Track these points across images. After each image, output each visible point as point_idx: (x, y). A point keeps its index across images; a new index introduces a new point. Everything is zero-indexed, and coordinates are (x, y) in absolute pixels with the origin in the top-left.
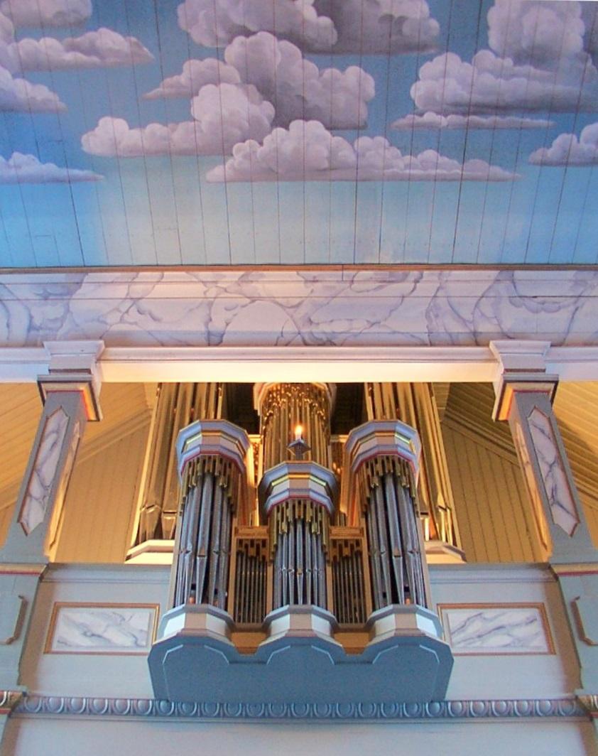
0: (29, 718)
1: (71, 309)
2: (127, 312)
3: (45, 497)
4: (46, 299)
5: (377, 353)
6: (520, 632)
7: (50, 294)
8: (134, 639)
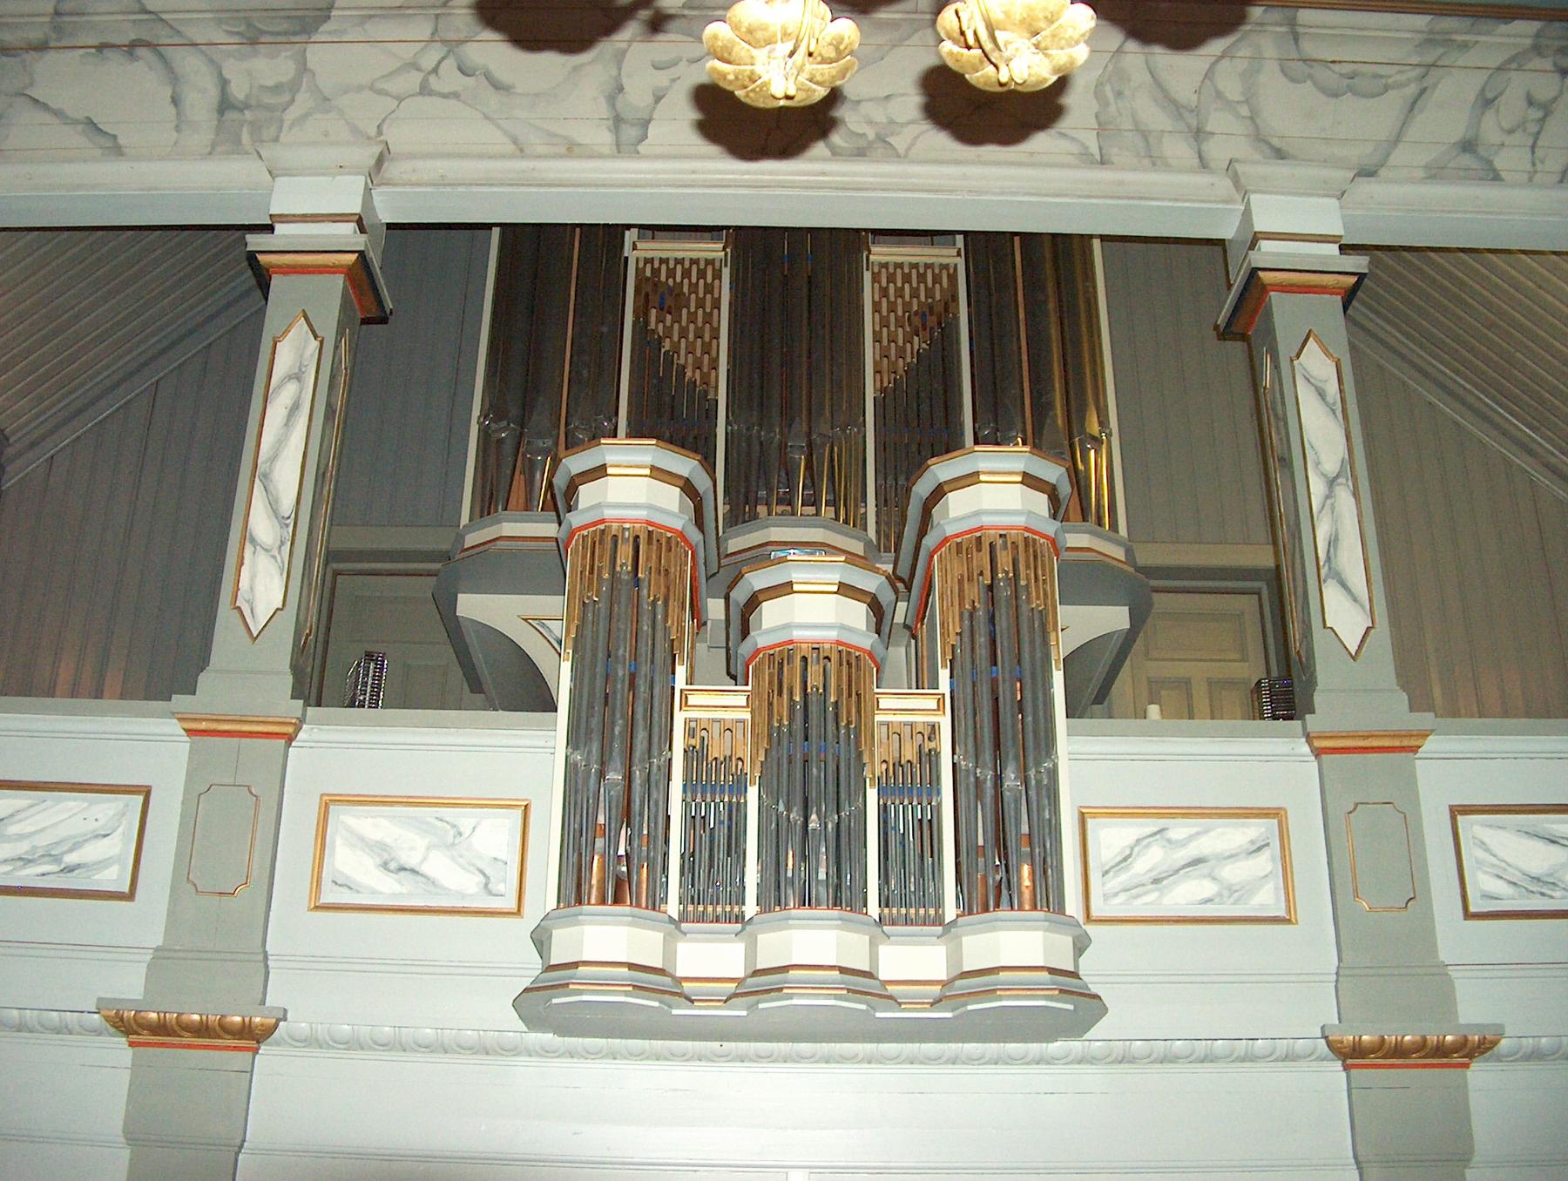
1: (309, 65)
2: (435, 70)
6: (1235, 872)
7: (263, 32)
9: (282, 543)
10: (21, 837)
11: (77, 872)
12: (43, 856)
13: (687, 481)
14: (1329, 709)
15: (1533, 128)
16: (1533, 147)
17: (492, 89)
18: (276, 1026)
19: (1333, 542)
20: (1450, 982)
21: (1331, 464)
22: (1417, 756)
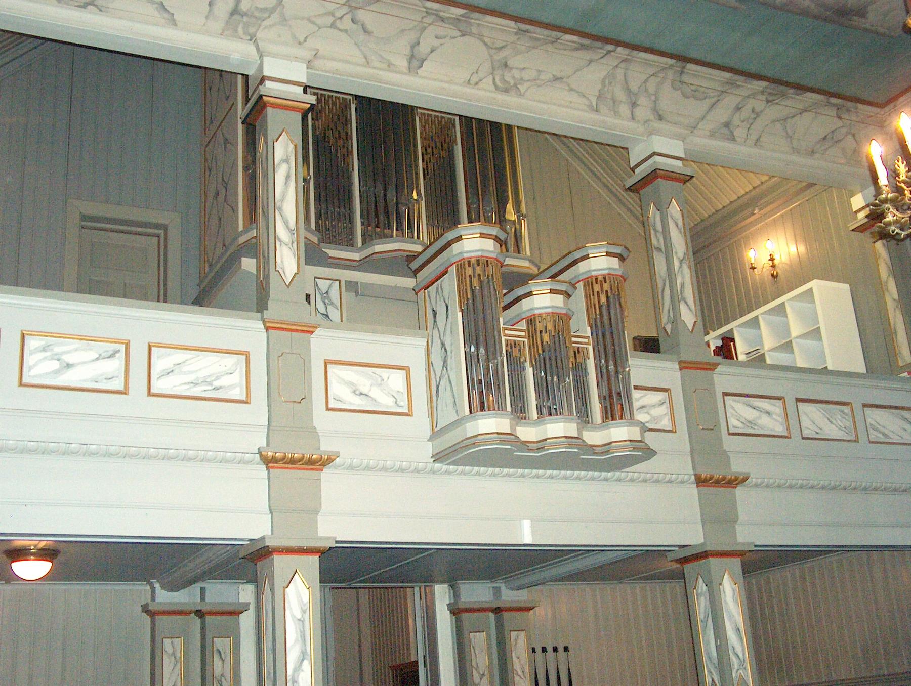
2: (341, 18)
9: (293, 243)
10: (191, 372)
11: (220, 390)
12: (202, 382)
13: (496, 236)
14: (274, 311)
15: (750, 121)
16: (748, 129)
18: (335, 459)
19: (683, 285)
20: (729, 457)
21: (681, 255)
22: (312, 336)
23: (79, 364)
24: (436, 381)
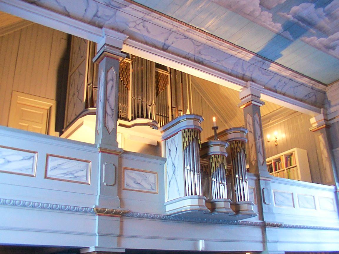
0: (125, 218)
3: (113, 115)
4: (108, 6)
5: (216, 73)
7: (111, 5)
8: (151, 186)
11: (77, 178)
12: (70, 173)
17: (146, 31)
19: (259, 147)
23: (14, 161)
24: (169, 180)
